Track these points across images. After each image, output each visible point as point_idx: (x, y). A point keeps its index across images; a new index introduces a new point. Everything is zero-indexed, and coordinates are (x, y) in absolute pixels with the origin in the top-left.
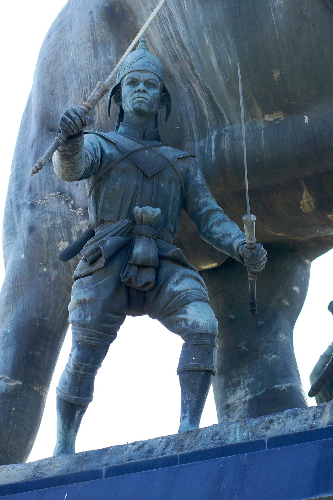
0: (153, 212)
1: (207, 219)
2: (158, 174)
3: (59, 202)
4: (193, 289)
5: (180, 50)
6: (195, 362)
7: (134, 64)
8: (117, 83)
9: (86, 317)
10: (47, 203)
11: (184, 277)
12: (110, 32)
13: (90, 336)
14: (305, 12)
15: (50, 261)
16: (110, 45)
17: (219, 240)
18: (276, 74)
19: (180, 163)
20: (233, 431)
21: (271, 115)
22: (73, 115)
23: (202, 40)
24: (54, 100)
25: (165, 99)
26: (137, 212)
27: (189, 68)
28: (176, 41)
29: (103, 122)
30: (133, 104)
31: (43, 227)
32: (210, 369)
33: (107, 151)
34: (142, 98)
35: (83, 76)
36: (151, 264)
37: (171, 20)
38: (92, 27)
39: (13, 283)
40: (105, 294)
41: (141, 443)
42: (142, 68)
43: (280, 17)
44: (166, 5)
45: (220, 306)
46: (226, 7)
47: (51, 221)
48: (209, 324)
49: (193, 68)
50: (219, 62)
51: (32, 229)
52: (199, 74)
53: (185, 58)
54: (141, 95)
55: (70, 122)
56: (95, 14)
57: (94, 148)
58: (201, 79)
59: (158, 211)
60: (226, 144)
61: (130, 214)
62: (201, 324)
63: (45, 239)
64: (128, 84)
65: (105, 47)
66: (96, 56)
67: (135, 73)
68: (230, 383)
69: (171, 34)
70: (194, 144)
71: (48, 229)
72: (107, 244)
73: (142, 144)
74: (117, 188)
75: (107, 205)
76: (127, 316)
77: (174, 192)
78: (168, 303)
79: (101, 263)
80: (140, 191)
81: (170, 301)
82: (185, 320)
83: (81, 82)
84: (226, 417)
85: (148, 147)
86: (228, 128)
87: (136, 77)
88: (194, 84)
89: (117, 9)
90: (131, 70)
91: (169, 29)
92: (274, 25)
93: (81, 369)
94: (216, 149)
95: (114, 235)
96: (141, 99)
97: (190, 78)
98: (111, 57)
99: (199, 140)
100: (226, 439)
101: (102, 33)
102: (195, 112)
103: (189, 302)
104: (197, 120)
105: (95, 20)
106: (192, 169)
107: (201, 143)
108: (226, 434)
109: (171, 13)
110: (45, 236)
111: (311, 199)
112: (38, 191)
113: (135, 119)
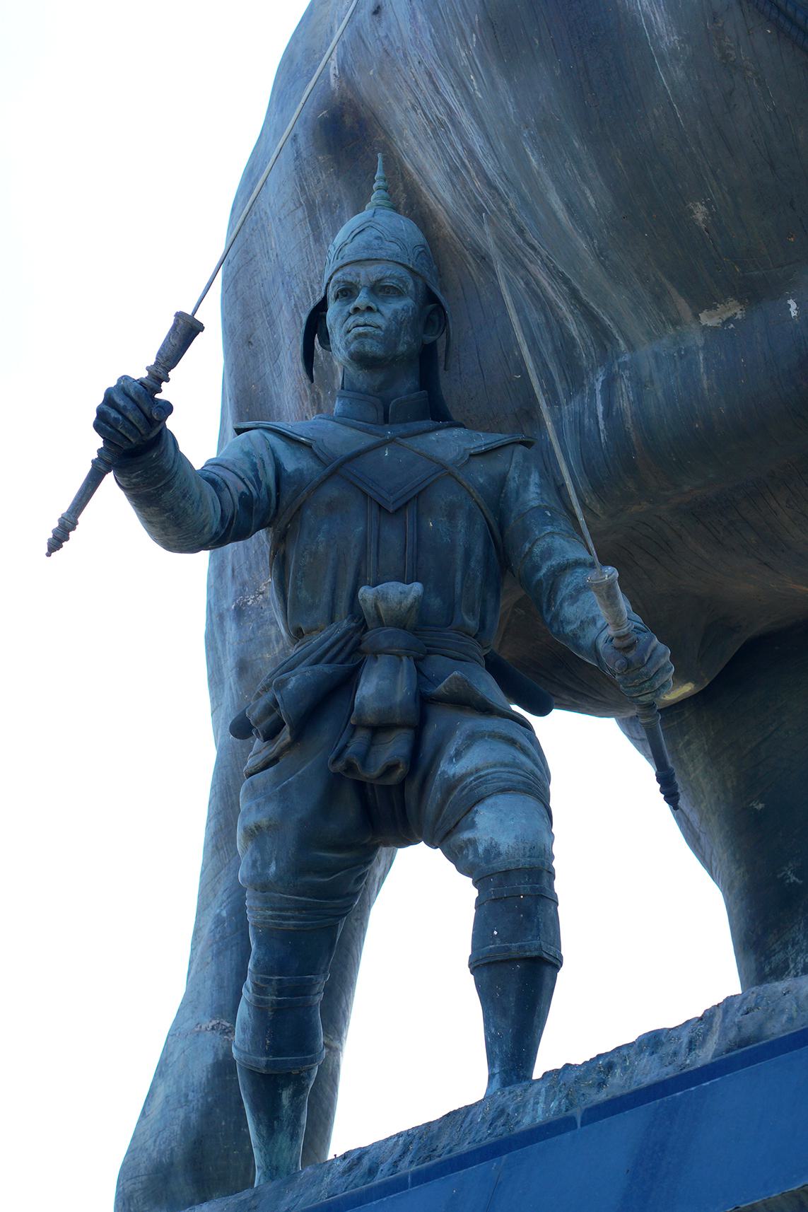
1: (554, 589)
2: (414, 502)
4: (494, 766)
5: (486, 194)
6: (498, 941)
7: (347, 248)
8: (318, 299)
9: (266, 865)
10: (266, 600)
11: (472, 738)
12: (338, 178)
13: (281, 910)
14: (732, 52)
16: (342, 208)
18: (700, 213)
19: (479, 465)
20: (532, 1102)
21: (712, 312)
22: (120, 402)
23: (522, 160)
24: (255, 355)
25: (435, 317)
26: (365, 601)
27: (513, 231)
28: (473, 174)
32: (535, 954)
33: (290, 465)
34: (365, 325)
35: (297, 290)
36: (398, 720)
37: (453, 125)
38: (299, 169)
39: (222, 798)
40: (303, 805)
41: (356, 1155)
42: (365, 256)
43: (679, 74)
44: (438, 92)
45: (729, 785)
46: (558, 73)
47: (278, 642)
48: (521, 846)
49: (521, 231)
50: (570, 207)
52: (535, 243)
53: (501, 210)
54: (361, 320)
55: (115, 419)
57: (254, 465)
58: (544, 253)
59: (417, 588)
60: (625, 402)
62: (503, 849)
64: (337, 297)
65: (332, 213)
66: (317, 239)
67: (347, 269)
68: (767, 969)
69: (460, 158)
70: (560, 409)
72: (289, 687)
73: (377, 435)
74: (321, 548)
75: (304, 594)
77: (460, 535)
79: (285, 736)
80: (372, 548)
81: (444, 801)
82: (472, 842)
83: (296, 305)
85: (392, 440)
86: (626, 358)
87: (349, 279)
88: (532, 267)
89: (348, 120)
90: (340, 262)
91: (454, 149)
92: (668, 97)
93: (270, 990)
94: (607, 414)
95: (316, 662)
96: (361, 329)
97: (521, 254)
99: (569, 398)
100: (518, 1123)
102: (551, 331)
103: (480, 800)
104: (556, 351)
105: (304, 155)
106: (514, 474)
107: (575, 405)
108: (517, 1110)
109: (450, 108)
112: (246, 576)
113: (361, 378)
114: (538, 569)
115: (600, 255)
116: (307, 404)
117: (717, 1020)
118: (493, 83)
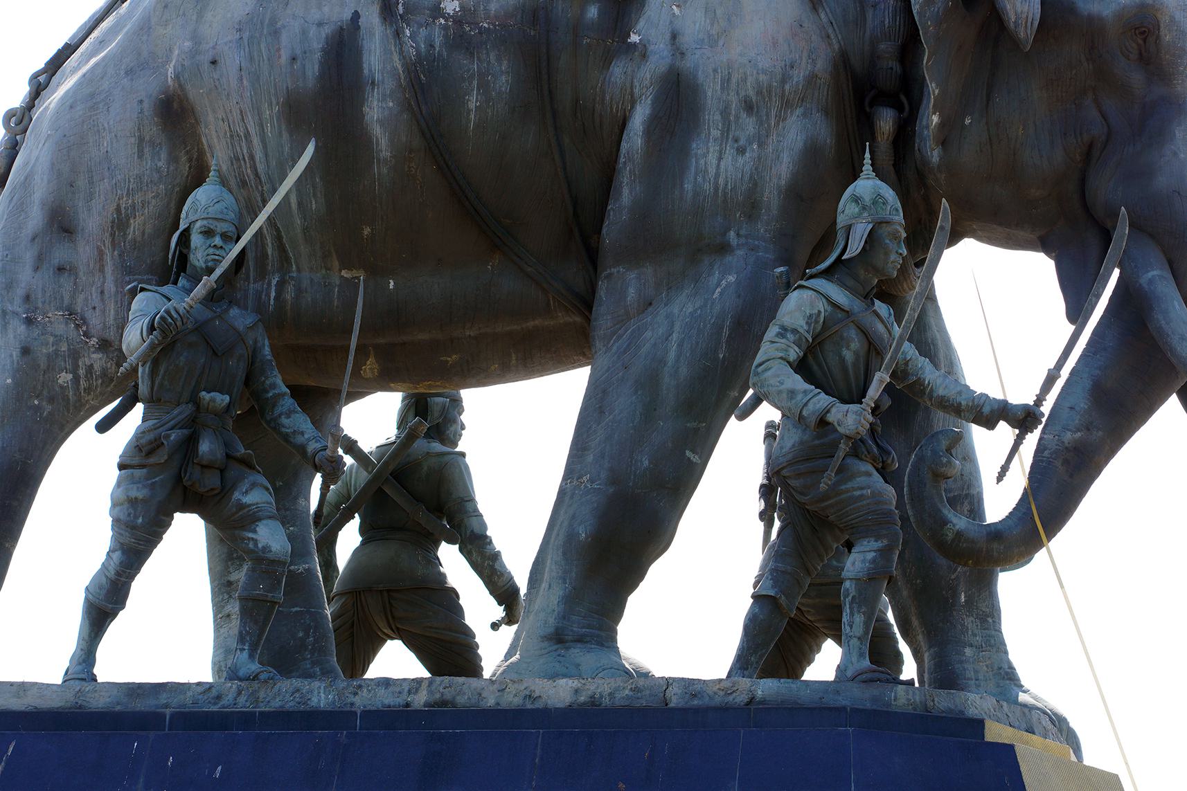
0: (222, 399)
1: (274, 405)
3: (67, 324)
9: (136, 517)
11: (254, 485)
15: (45, 393)
17: (287, 434)
18: (367, 231)
24: (73, 193)
29: (139, 239)
30: (206, 261)
31: (42, 352)
50: (300, 204)
51: (25, 351)
56: (146, 105)
60: (289, 294)
61: (195, 400)
62: (273, 549)
63: (43, 366)
66: (141, 156)
71: (49, 356)
76: (177, 515)
78: (233, 515)
84: (226, 596)
86: (294, 275)
89: (175, 105)
90: (205, 215)
98: (160, 164)
101: (152, 130)
103: (260, 520)
106: (260, 339)
107: (258, 286)
110: (43, 363)
111: (376, 366)
114: (267, 392)
115: (305, 230)
116: (107, 235)
117: (424, 685)
118: (280, 133)
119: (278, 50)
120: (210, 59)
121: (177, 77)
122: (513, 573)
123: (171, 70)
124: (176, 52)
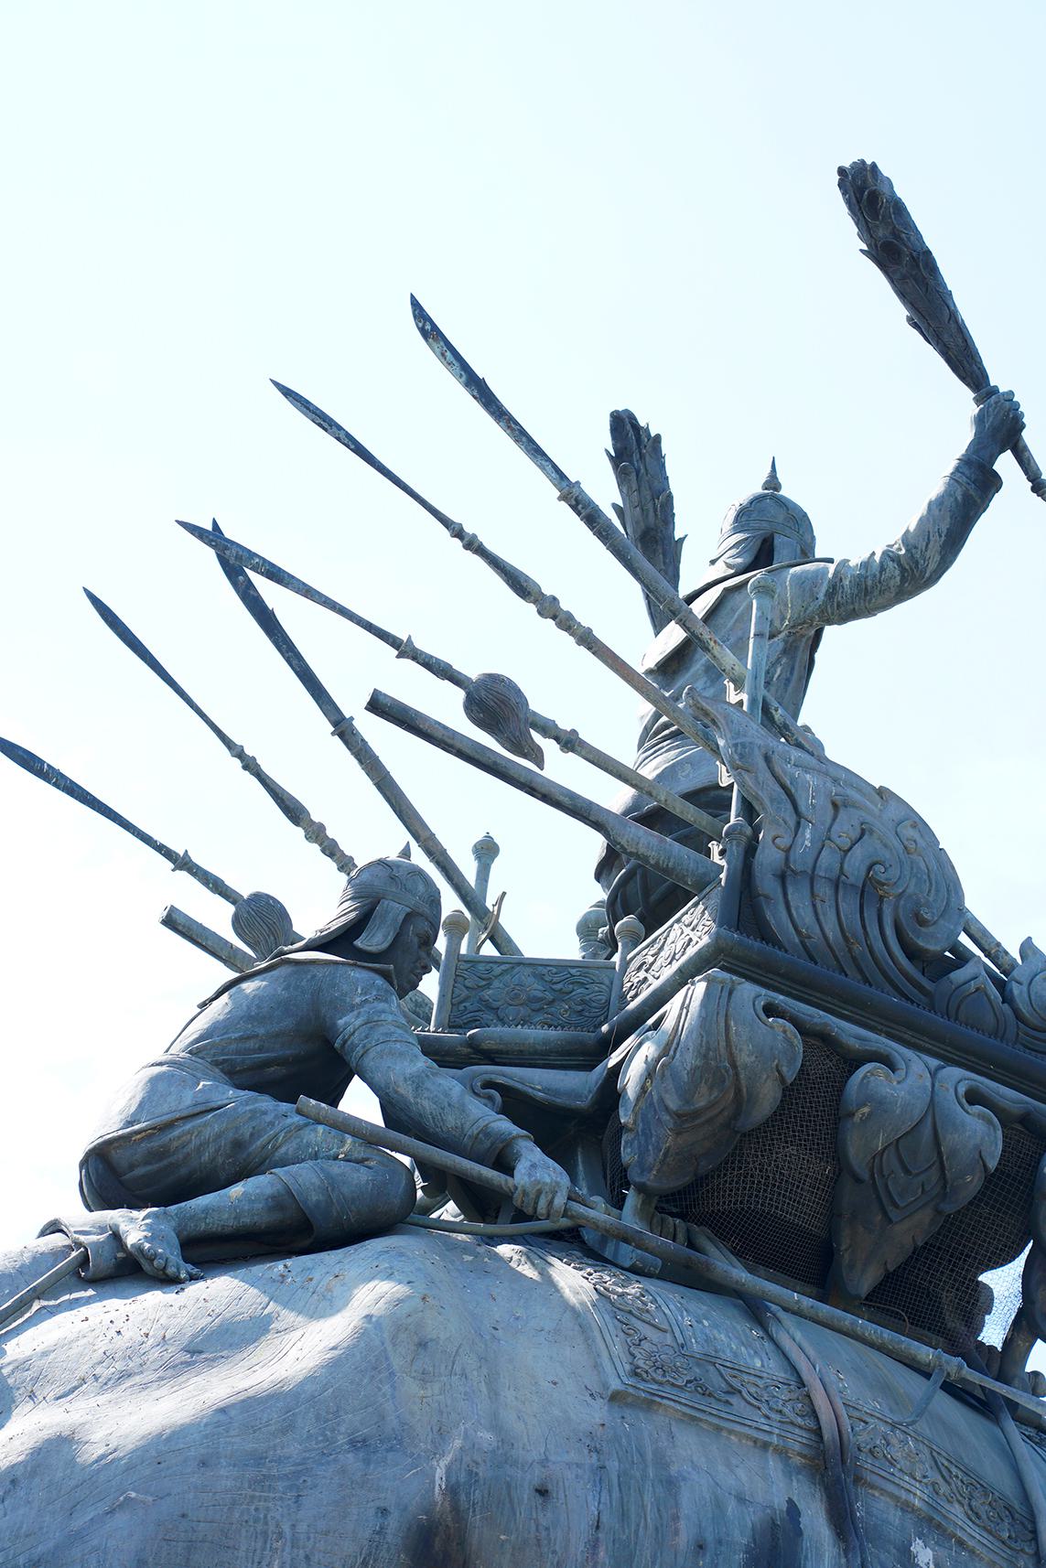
56: (393, 1523)
119: (676, 1518)
120: (536, 1482)
121: (452, 1490)
122: (950, 465)
123: (440, 1472)
124: (458, 1443)
